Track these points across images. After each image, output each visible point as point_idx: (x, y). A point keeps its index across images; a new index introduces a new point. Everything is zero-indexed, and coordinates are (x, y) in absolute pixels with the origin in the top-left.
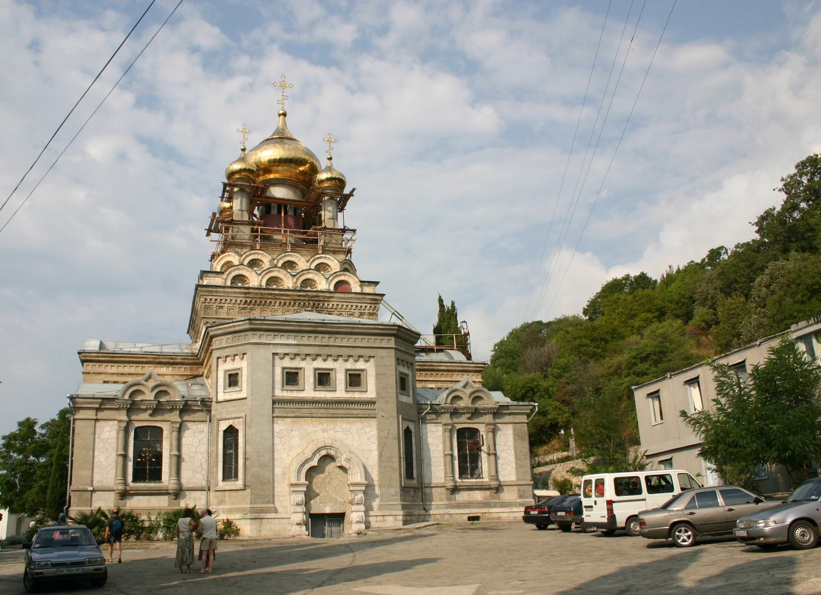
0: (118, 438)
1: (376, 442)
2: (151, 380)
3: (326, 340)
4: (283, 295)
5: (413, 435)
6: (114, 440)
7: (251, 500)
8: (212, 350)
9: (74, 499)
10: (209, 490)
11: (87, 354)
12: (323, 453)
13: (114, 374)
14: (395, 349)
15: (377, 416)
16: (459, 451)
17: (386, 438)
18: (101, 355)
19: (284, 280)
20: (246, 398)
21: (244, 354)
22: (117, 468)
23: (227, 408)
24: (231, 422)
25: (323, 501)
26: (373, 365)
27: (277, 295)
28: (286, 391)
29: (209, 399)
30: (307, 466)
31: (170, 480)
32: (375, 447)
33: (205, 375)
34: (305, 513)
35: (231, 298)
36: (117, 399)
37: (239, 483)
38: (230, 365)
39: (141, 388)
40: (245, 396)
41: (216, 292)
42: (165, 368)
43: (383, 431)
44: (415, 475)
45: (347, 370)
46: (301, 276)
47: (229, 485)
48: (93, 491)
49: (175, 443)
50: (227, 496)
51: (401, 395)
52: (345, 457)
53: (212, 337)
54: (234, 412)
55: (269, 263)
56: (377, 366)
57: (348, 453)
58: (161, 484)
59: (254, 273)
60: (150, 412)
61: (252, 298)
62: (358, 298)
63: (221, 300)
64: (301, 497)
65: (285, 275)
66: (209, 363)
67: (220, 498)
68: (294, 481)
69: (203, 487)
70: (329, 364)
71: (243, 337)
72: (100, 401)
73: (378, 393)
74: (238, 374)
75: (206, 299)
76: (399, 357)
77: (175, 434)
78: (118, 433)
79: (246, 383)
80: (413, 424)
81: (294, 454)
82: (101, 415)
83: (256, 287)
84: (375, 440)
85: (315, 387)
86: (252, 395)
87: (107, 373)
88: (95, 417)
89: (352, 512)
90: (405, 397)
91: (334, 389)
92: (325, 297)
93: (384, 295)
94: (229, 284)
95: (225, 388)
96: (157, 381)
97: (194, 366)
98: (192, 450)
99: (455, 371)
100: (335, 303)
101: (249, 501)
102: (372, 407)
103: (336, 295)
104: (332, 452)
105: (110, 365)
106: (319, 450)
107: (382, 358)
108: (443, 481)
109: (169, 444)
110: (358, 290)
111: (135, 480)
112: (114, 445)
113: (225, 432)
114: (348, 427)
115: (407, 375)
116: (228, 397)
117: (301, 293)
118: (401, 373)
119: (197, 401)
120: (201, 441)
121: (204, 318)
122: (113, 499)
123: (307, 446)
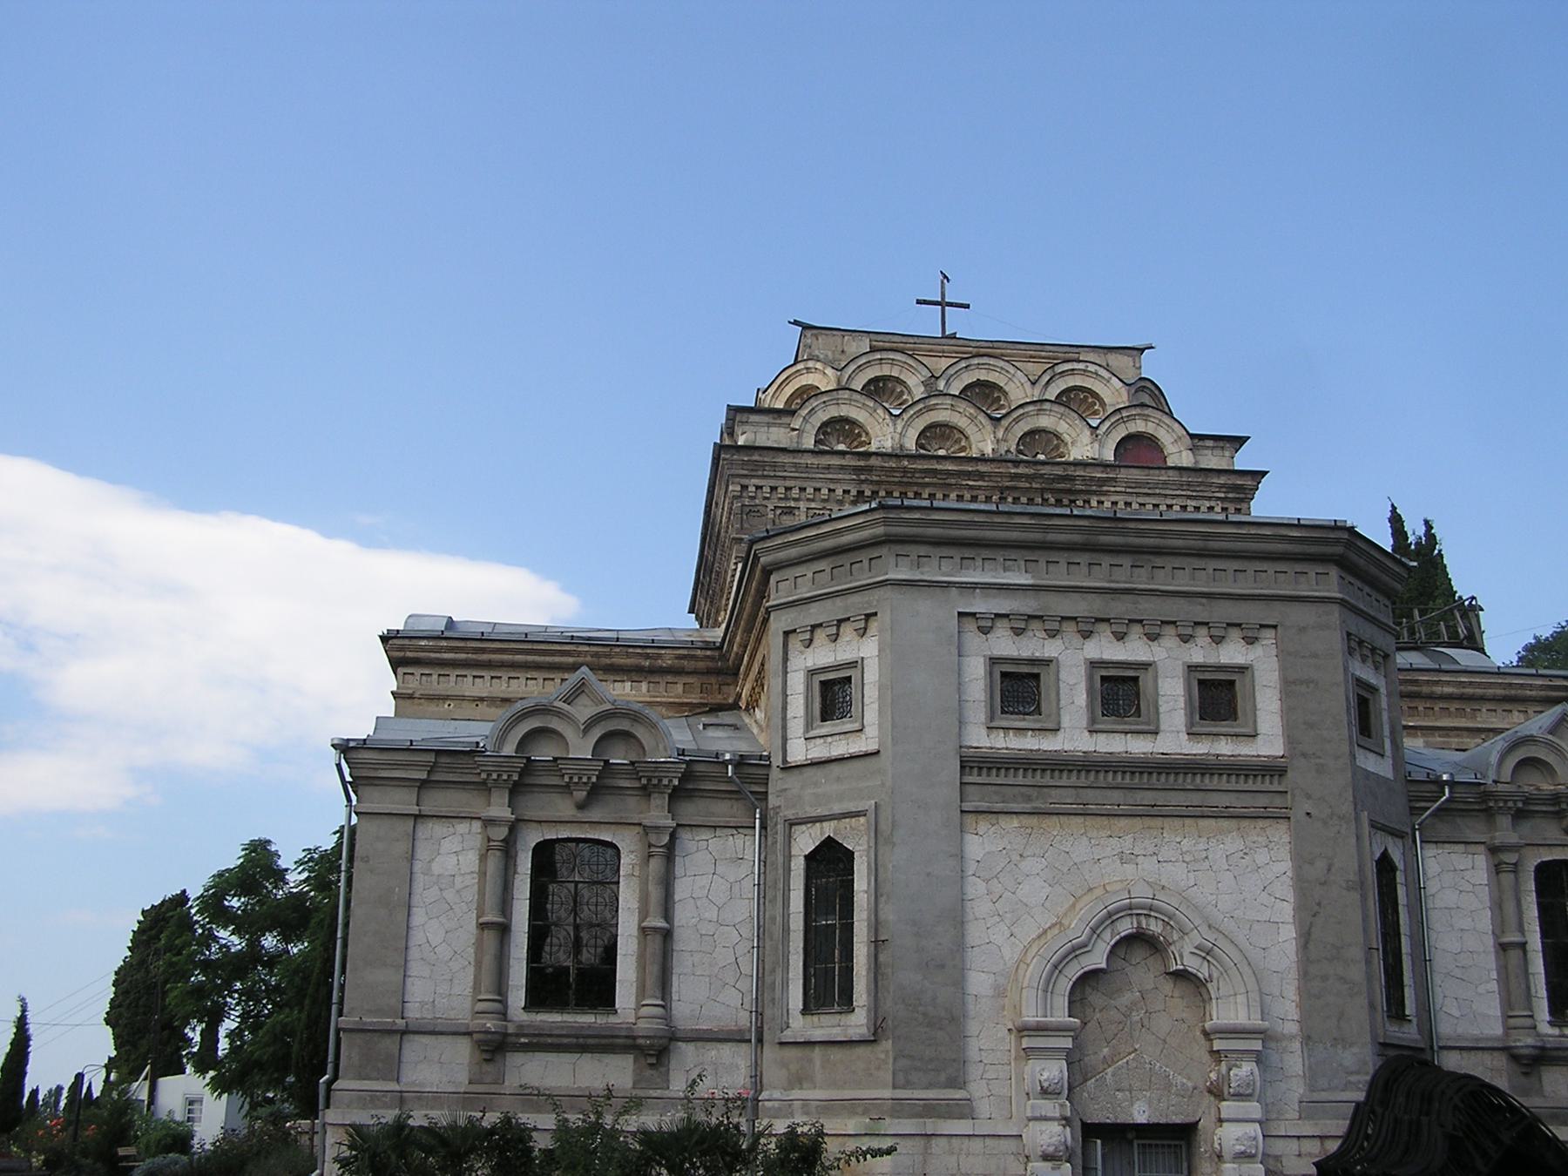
0: (482, 874)
1: (1291, 897)
2: (583, 699)
3: (1124, 574)
4: (968, 475)
5: (1400, 877)
6: (473, 881)
7: (894, 1074)
8: (768, 613)
9: (349, 1058)
10: (760, 1040)
11: (406, 642)
12: (1126, 927)
13: (482, 699)
14: (1343, 603)
15: (1291, 813)
16: (1544, 935)
17: (1324, 884)
18: (444, 643)
19: (969, 432)
20: (878, 752)
21: (868, 617)
22: (478, 964)
23: (816, 784)
24: (828, 829)
25: (1125, 1084)
26: (1274, 652)
27: (949, 473)
28: (1001, 734)
29: (761, 757)
30: (1074, 971)
31: (639, 1006)
32: (1287, 911)
33: (743, 704)
34: (1066, 1121)
36: (481, 753)
37: (857, 1022)
38: (823, 655)
39: (555, 723)
40: (873, 747)
41: (774, 466)
42: (628, 684)
43: (1311, 863)
44: (1410, 1009)
45: (1192, 668)
46: (1017, 420)
47: (825, 1027)
48: (404, 1032)
49: (655, 893)
50: (818, 1063)
51: (1361, 750)
52: (1198, 940)
53: (767, 573)
55: (922, 389)
56: (1283, 655)
57: (1204, 929)
58: (612, 1019)
59: (880, 411)
60: (581, 795)
61: (878, 483)
62: (1189, 484)
63: (788, 489)
64: (1053, 1071)
65: (972, 419)
66: (759, 658)
68: (1031, 1016)
70: (1135, 650)
71: (866, 563)
73: (1290, 740)
74: (849, 679)
75: (744, 487)
76: (1353, 630)
77: (656, 865)
78: (483, 858)
79: (876, 706)
80: (1399, 842)
81: (1029, 930)
82: (436, 801)
83: (890, 450)
84: (1285, 889)
85: (1093, 720)
86: (895, 741)
87: (462, 698)
88: (414, 810)
89: (1221, 1121)
90: (1371, 756)
91: (1152, 728)
92: (1092, 478)
93: (1264, 473)
94: (809, 443)
95: (809, 725)
96: (602, 702)
97: (713, 680)
98: (707, 915)
99: (1482, 699)
100: (1121, 499)
101: (889, 1078)
102: (1275, 787)
103: (1123, 474)
104: (1155, 927)
105: (470, 673)
106: (1111, 917)
107: (1302, 630)
108: (1498, 1030)
109: (637, 895)
110: (1186, 460)
112: (471, 895)
113: (809, 858)
114: (1202, 846)
115: (1373, 689)
116: (819, 751)
117: (1021, 470)
118: (1360, 682)
119: (725, 763)
120: (736, 888)
122: (466, 1061)
123: (1074, 905)
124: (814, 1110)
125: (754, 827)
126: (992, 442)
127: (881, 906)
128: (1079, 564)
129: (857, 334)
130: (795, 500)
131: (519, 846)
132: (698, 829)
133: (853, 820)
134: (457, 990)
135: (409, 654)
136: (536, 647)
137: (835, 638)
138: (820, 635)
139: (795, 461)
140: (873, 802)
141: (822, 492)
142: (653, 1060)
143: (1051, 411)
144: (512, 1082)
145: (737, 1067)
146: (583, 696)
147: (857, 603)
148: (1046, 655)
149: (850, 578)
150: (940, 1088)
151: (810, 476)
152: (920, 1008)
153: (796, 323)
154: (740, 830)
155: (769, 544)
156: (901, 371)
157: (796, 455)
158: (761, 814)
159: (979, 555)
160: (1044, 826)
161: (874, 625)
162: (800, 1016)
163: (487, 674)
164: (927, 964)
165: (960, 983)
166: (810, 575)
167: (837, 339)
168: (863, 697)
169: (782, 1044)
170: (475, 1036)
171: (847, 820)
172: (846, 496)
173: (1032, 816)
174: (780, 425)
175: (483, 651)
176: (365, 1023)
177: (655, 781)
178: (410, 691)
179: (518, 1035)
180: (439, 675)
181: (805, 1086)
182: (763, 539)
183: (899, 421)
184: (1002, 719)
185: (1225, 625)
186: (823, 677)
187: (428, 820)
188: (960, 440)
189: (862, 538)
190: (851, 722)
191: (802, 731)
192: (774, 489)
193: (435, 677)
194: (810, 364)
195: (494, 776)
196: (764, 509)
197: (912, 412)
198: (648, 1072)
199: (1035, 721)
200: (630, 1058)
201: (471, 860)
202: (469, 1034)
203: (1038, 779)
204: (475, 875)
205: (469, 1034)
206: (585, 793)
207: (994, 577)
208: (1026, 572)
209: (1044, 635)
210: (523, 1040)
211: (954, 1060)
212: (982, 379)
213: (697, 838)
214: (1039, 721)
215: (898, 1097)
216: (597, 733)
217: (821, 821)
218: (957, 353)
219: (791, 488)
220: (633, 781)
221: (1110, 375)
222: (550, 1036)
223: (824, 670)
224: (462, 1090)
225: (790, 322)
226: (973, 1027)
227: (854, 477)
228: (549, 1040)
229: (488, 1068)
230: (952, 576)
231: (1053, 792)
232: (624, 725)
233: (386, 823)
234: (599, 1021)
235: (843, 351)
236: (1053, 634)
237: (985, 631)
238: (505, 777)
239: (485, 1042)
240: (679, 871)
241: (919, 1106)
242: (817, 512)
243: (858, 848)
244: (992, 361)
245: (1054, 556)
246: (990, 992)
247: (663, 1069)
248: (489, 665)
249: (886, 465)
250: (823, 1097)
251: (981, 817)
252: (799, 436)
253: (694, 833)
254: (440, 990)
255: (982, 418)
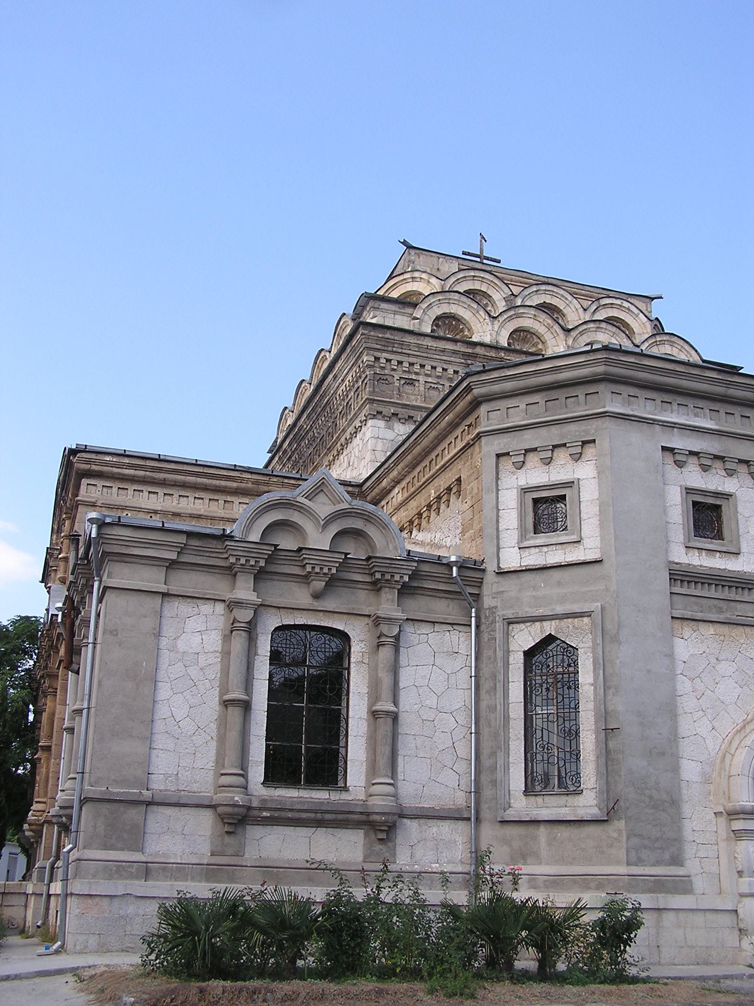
0: (226, 654)
2: (321, 498)
6: (215, 660)
11: (93, 456)
18: (126, 460)
21: (584, 443)
23: (534, 588)
24: (549, 628)
28: (696, 552)
35: (434, 364)
39: (295, 517)
41: (402, 344)
46: (581, 333)
53: (476, 404)
54: (562, 600)
58: (344, 796)
60: (319, 585)
63: (412, 364)
65: (549, 328)
67: (516, 844)
69: (459, 810)
72: (182, 539)
74: (563, 498)
75: (377, 359)
78: (227, 638)
79: (595, 521)
82: (184, 581)
88: (163, 588)
95: (523, 536)
101: (622, 854)
105: (146, 488)
111: (272, 776)
112: (215, 672)
116: (533, 559)
119: (449, 566)
120: (453, 679)
121: (371, 401)
122: (208, 833)
124: (541, 885)
125: (470, 626)
126: (564, 347)
127: (609, 698)
128: (749, 417)
129: (449, 258)
130: (417, 374)
131: (259, 630)
132: (420, 623)
133: (576, 620)
134: (199, 764)
135: (94, 467)
136: (206, 470)
137: (548, 461)
138: (533, 459)
139: (418, 342)
140: (599, 604)
141: (438, 369)
142: (383, 836)
143: (606, 329)
144: (251, 854)
145: (455, 842)
146: (321, 495)
147: (574, 432)
148: (727, 490)
149: (564, 410)
150: (666, 865)
151: (429, 356)
152: (647, 792)
153: (404, 243)
154: (455, 627)
155: (484, 377)
156: (488, 288)
157: (419, 337)
158: (476, 613)
159: (675, 401)
160: (733, 634)
161: (590, 451)
162: (523, 798)
163: (161, 491)
164: (650, 752)
165: (676, 769)
166: (523, 406)
167: (434, 259)
168: (580, 513)
169: (503, 822)
170: (220, 810)
171: (570, 620)
172: (456, 375)
173: (724, 625)
174: (403, 314)
175: (160, 470)
176: (112, 793)
177: (388, 577)
178: (94, 500)
179: (260, 809)
180: (119, 488)
181: (529, 861)
182: (479, 373)
183: (496, 322)
184: (695, 541)
185: (712, 457)
186: (536, 495)
187: (174, 599)
188: (537, 343)
189: (581, 375)
190: (567, 535)
191: (516, 541)
192: (400, 363)
193: (115, 490)
194: (416, 274)
195: (243, 561)
196: (391, 377)
197: (505, 317)
198: (378, 847)
199: (719, 544)
200: (360, 834)
201: (214, 640)
202: (213, 807)
203: (726, 594)
204: (218, 654)
205: (213, 807)
206: (324, 583)
207: (688, 420)
208: (711, 419)
209: (724, 473)
210: (265, 814)
211: (676, 840)
212: (547, 302)
213: (418, 632)
214: (723, 545)
215: (634, 873)
216: (334, 529)
217: (541, 621)
218: (521, 283)
219: (413, 364)
220: (365, 576)
221: (639, 312)
222: (291, 810)
223: (538, 488)
224: (205, 862)
225: (400, 241)
226: (686, 809)
227: (463, 361)
228: (290, 815)
229: (228, 839)
230: (654, 415)
231: (739, 606)
232: (358, 524)
233: (133, 599)
234: (332, 798)
235: (438, 269)
236: (730, 473)
237: (680, 464)
238: (252, 562)
239: (230, 815)
240: (403, 660)
241: (651, 881)
242: (433, 385)
243: (581, 645)
244: (555, 289)
245: (731, 409)
246: (699, 779)
247: (390, 844)
248: (163, 483)
249: (488, 354)
250: (552, 872)
251: (686, 623)
252: (420, 324)
253: (416, 626)
254: (183, 763)
255: (557, 328)
